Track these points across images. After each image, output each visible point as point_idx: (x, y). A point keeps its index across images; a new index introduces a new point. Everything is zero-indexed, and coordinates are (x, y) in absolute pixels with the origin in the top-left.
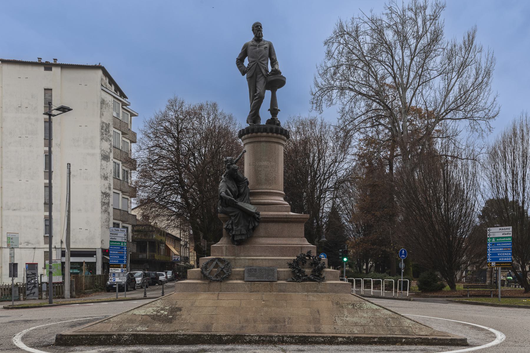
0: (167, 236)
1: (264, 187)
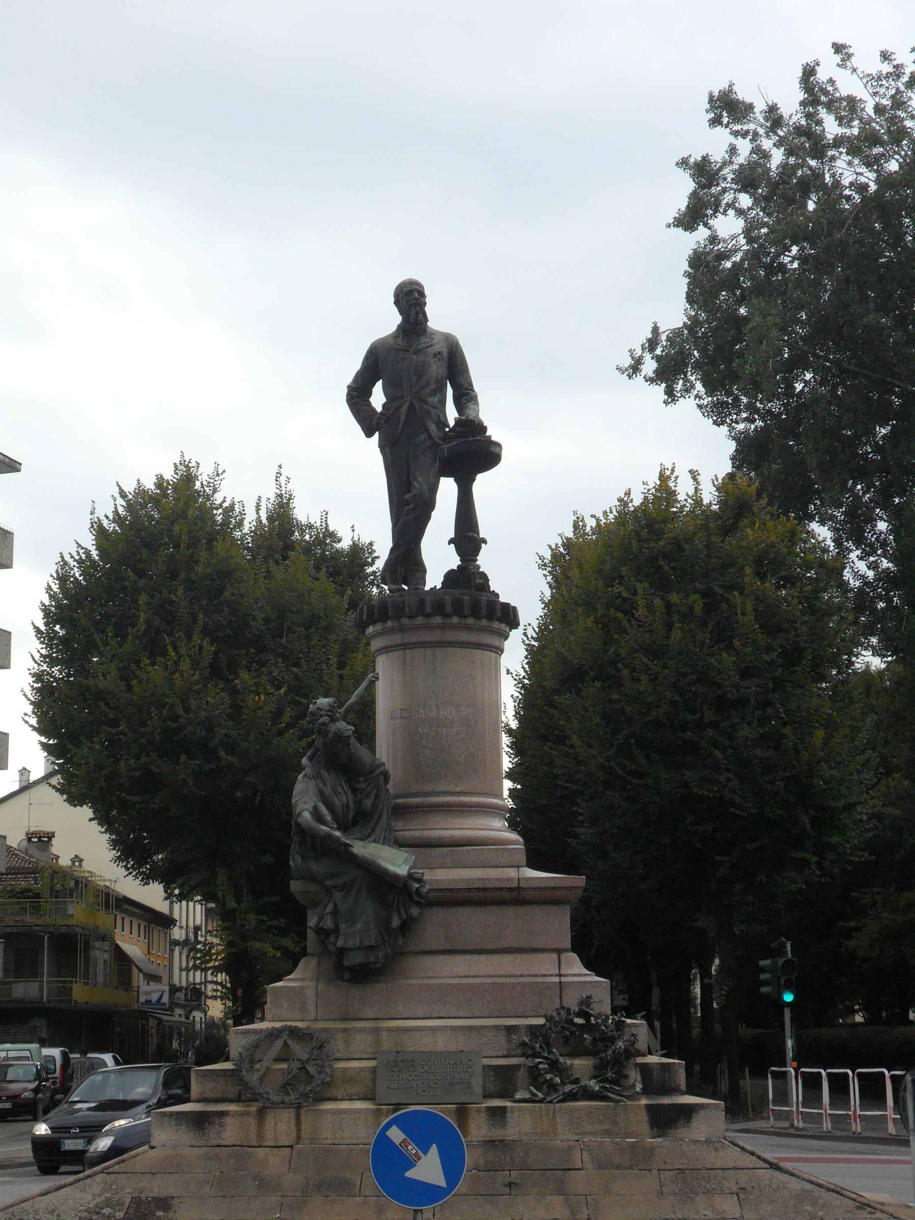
0: (118, 907)
1: (440, 787)
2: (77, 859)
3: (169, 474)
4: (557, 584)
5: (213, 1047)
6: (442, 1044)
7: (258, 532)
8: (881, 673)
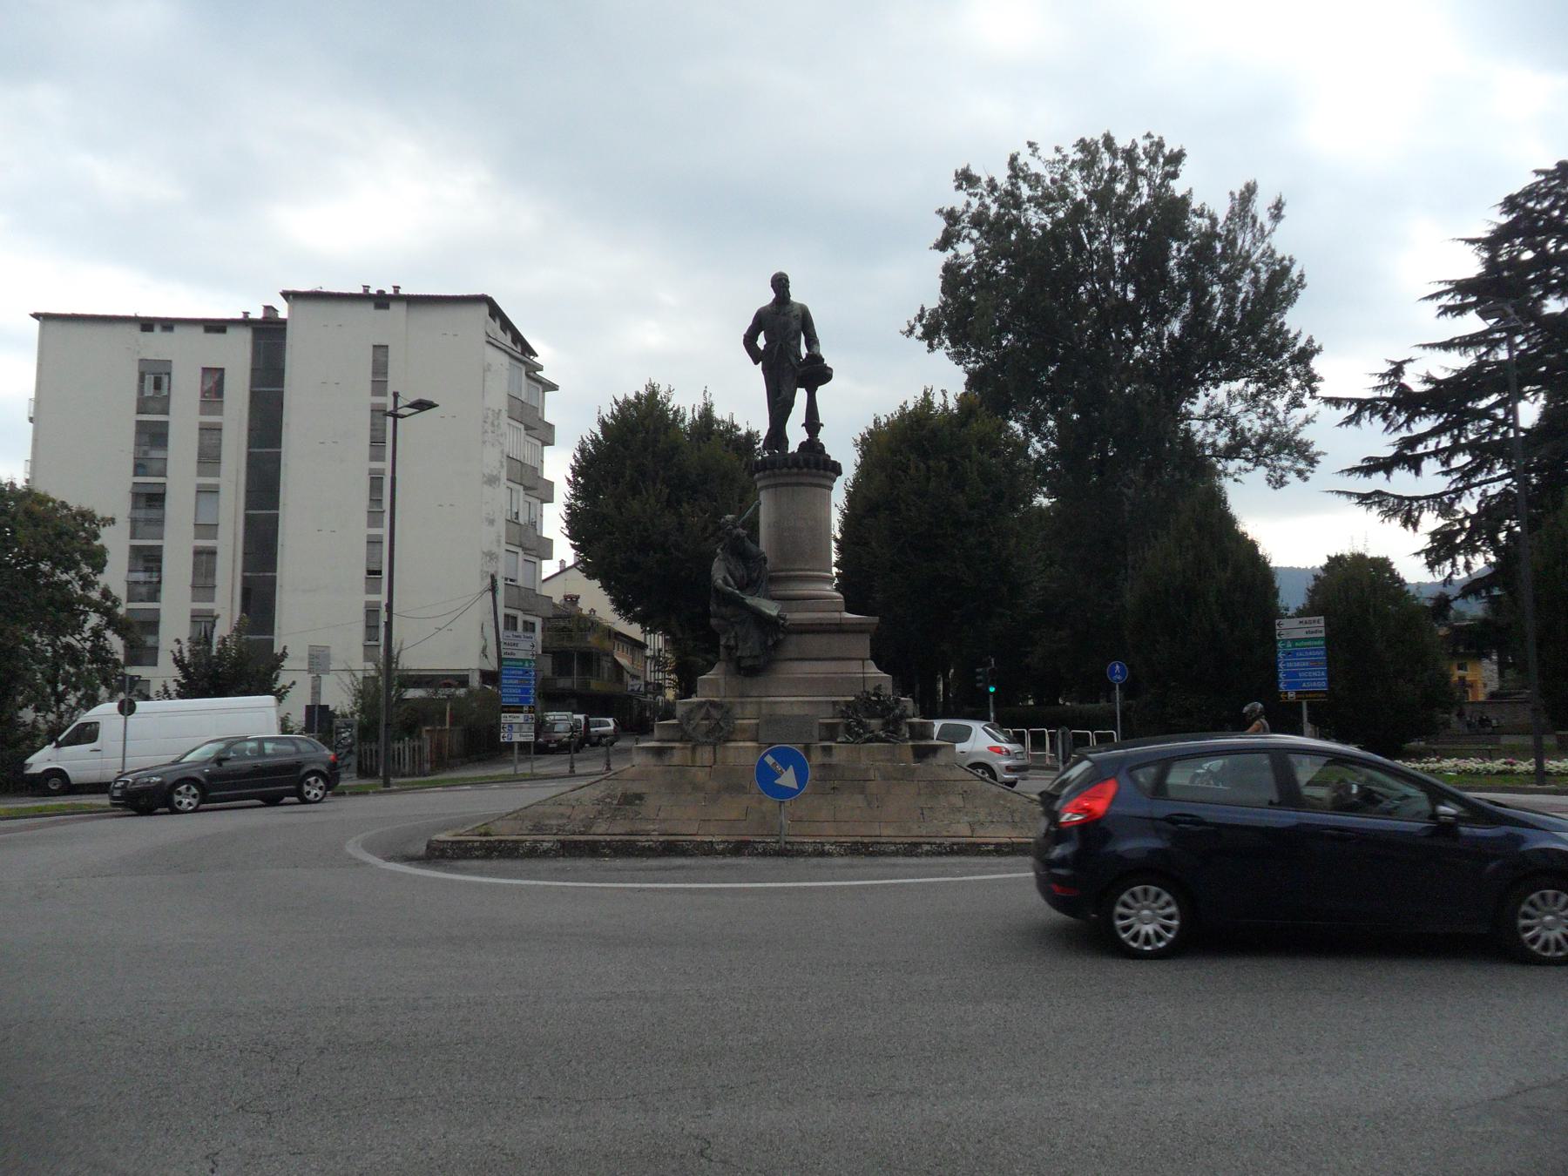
2: (593, 610)
3: (643, 391)
4: (864, 456)
5: (668, 711)
6: (796, 711)
7: (694, 424)
8: (1048, 508)
